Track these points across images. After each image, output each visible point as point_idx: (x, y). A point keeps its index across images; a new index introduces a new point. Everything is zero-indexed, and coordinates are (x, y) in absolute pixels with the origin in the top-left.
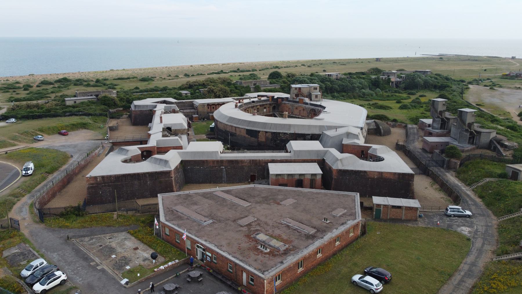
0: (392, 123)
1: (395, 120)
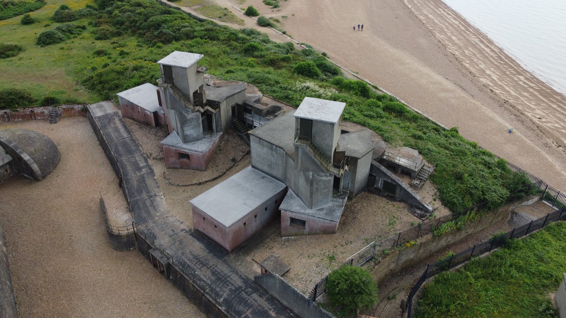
0: (47, 110)
1: (49, 101)
